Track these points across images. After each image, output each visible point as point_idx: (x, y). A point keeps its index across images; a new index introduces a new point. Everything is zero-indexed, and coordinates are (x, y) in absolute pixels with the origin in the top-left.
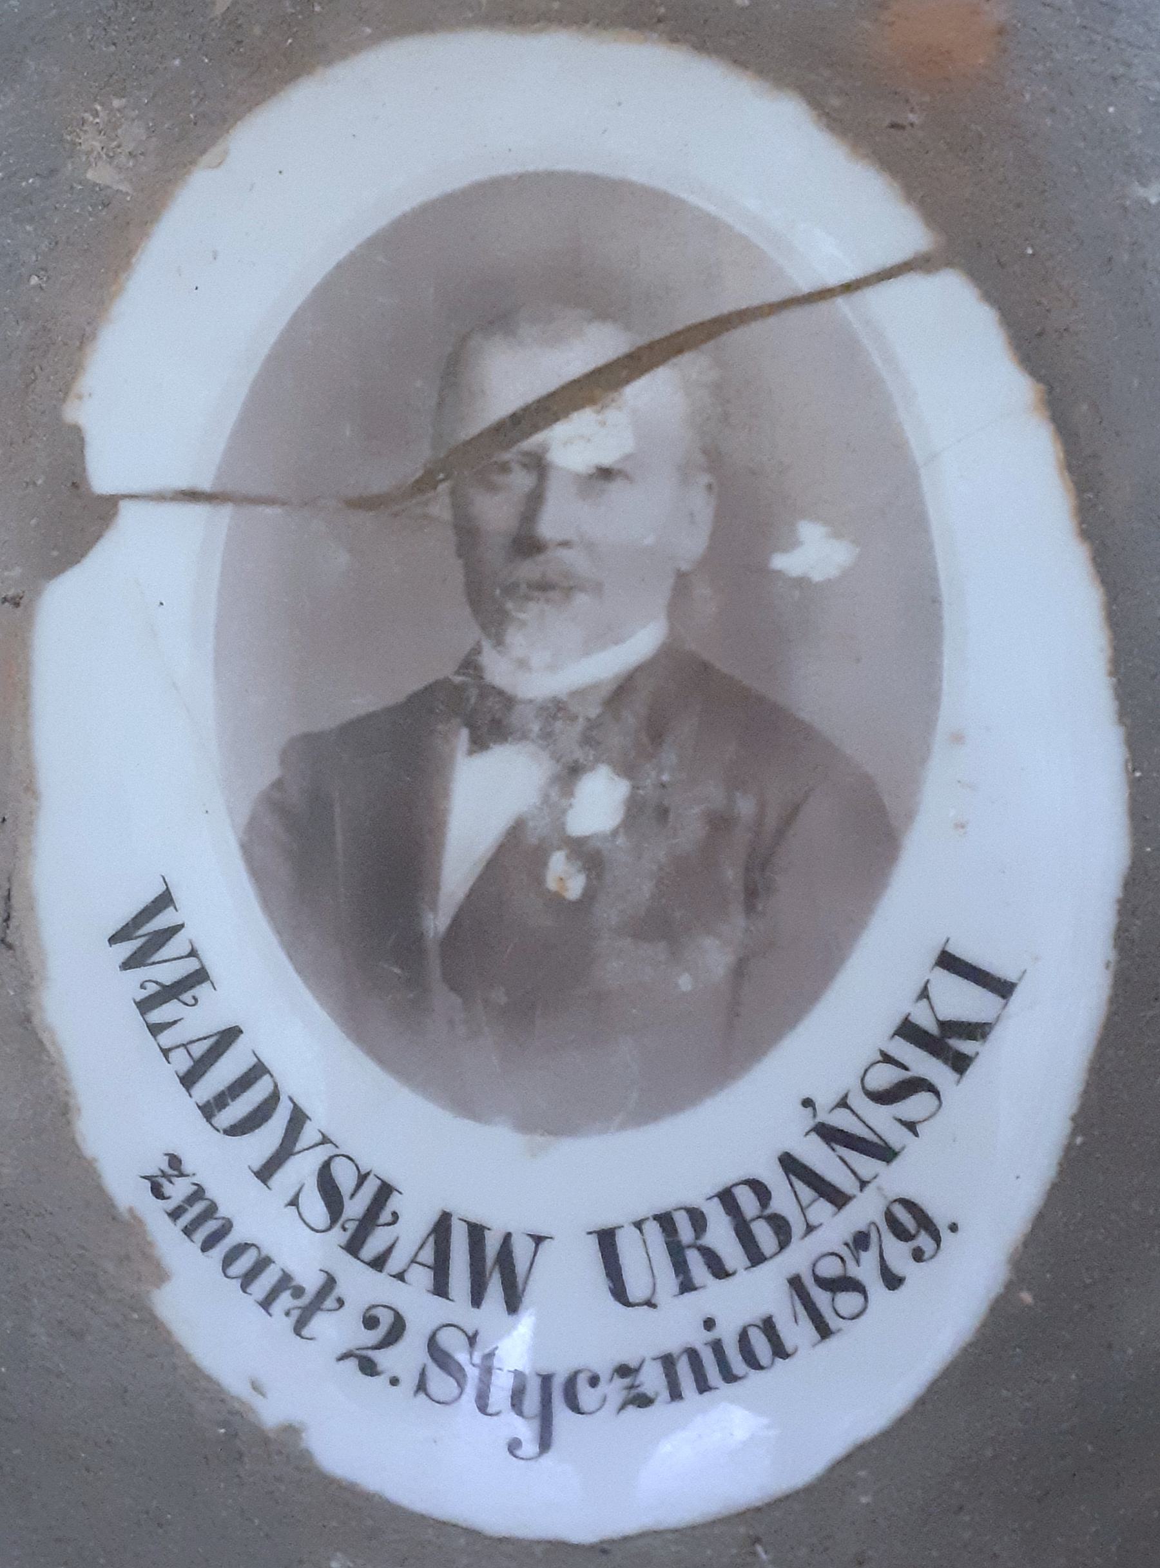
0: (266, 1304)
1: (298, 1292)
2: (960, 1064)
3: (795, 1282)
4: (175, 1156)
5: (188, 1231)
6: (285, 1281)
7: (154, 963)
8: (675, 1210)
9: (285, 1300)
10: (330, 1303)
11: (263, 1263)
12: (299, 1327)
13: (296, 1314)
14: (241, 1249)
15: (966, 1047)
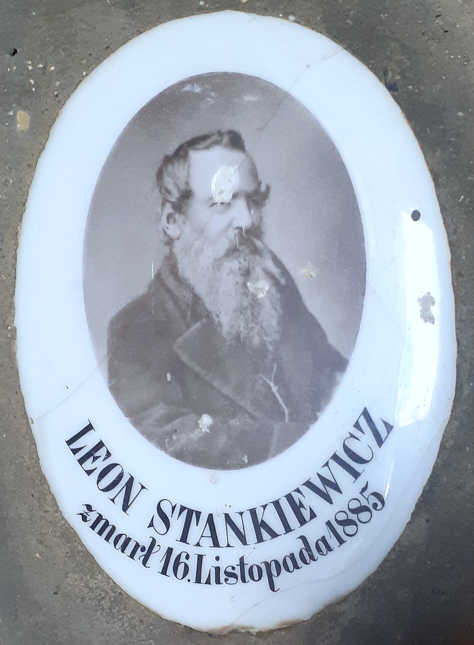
0: (132, 556)
1: (143, 549)
3: (329, 524)
4: (88, 505)
5: (100, 533)
7: (327, 492)
8: (355, 481)
9: (139, 553)
10: (156, 548)
11: (128, 540)
12: (144, 563)
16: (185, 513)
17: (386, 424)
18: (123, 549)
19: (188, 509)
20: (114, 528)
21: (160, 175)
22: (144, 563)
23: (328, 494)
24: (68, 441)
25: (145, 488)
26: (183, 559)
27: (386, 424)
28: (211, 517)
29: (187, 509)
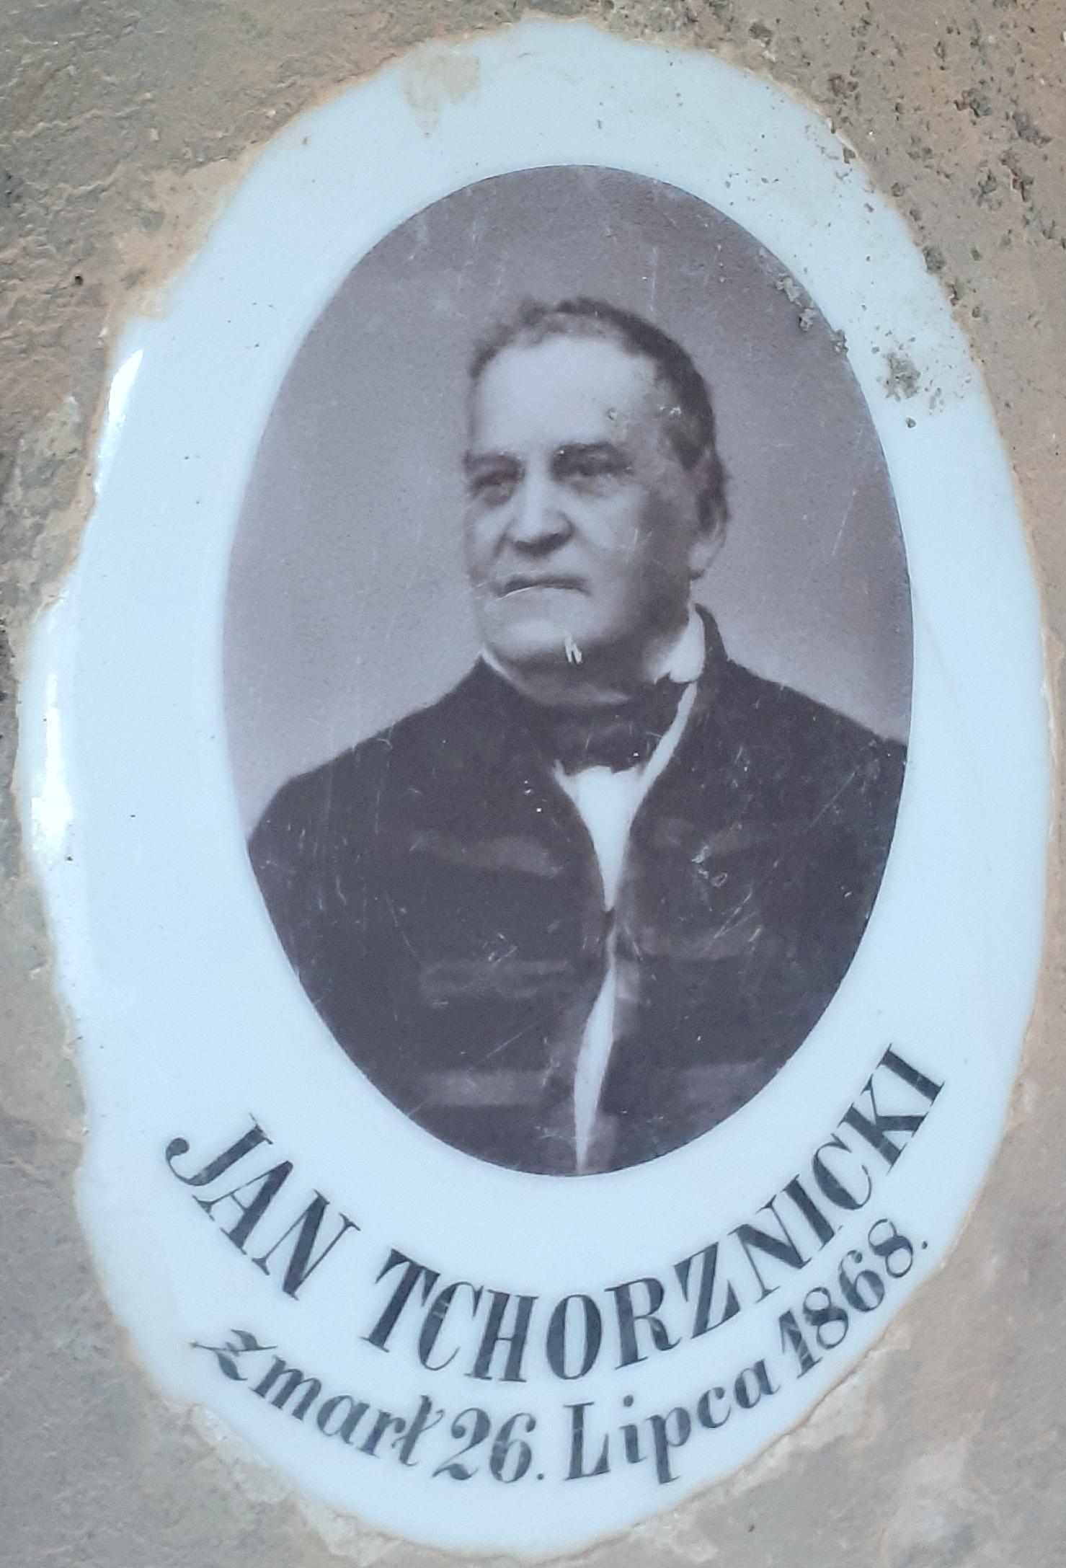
1: (400, 1425)
2: (892, 1154)
6: (384, 1418)
9: (389, 1435)
10: (432, 1417)
11: (359, 1410)
12: (404, 1458)
13: (400, 1445)
14: (330, 1406)
15: (897, 1137)
16: (399, 1271)
17: (732, 1297)
18: (346, 1432)
19: (411, 1262)
20: (316, 1387)
21: (817, 1290)
22: (404, 1458)
23: (790, 1240)
24: (531, 1304)
25: (352, 1225)
26: (518, 1432)
27: (732, 1297)
28: (280, 1174)
29: (406, 1264)
